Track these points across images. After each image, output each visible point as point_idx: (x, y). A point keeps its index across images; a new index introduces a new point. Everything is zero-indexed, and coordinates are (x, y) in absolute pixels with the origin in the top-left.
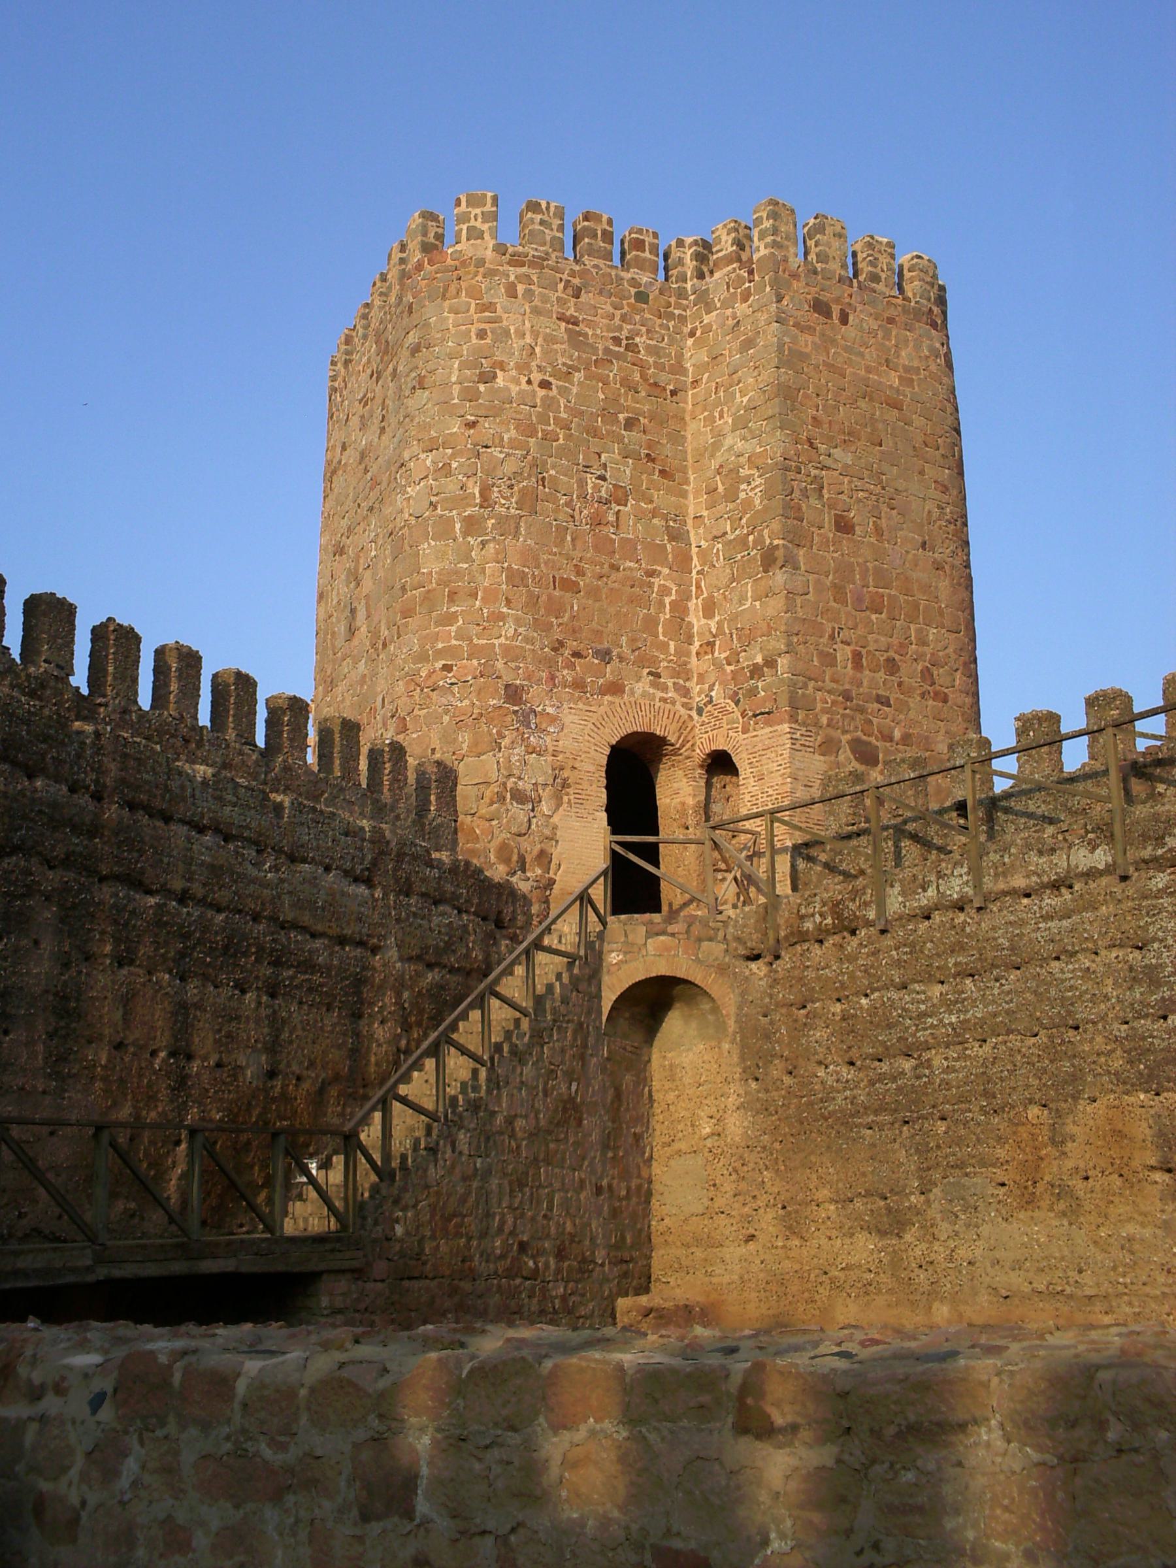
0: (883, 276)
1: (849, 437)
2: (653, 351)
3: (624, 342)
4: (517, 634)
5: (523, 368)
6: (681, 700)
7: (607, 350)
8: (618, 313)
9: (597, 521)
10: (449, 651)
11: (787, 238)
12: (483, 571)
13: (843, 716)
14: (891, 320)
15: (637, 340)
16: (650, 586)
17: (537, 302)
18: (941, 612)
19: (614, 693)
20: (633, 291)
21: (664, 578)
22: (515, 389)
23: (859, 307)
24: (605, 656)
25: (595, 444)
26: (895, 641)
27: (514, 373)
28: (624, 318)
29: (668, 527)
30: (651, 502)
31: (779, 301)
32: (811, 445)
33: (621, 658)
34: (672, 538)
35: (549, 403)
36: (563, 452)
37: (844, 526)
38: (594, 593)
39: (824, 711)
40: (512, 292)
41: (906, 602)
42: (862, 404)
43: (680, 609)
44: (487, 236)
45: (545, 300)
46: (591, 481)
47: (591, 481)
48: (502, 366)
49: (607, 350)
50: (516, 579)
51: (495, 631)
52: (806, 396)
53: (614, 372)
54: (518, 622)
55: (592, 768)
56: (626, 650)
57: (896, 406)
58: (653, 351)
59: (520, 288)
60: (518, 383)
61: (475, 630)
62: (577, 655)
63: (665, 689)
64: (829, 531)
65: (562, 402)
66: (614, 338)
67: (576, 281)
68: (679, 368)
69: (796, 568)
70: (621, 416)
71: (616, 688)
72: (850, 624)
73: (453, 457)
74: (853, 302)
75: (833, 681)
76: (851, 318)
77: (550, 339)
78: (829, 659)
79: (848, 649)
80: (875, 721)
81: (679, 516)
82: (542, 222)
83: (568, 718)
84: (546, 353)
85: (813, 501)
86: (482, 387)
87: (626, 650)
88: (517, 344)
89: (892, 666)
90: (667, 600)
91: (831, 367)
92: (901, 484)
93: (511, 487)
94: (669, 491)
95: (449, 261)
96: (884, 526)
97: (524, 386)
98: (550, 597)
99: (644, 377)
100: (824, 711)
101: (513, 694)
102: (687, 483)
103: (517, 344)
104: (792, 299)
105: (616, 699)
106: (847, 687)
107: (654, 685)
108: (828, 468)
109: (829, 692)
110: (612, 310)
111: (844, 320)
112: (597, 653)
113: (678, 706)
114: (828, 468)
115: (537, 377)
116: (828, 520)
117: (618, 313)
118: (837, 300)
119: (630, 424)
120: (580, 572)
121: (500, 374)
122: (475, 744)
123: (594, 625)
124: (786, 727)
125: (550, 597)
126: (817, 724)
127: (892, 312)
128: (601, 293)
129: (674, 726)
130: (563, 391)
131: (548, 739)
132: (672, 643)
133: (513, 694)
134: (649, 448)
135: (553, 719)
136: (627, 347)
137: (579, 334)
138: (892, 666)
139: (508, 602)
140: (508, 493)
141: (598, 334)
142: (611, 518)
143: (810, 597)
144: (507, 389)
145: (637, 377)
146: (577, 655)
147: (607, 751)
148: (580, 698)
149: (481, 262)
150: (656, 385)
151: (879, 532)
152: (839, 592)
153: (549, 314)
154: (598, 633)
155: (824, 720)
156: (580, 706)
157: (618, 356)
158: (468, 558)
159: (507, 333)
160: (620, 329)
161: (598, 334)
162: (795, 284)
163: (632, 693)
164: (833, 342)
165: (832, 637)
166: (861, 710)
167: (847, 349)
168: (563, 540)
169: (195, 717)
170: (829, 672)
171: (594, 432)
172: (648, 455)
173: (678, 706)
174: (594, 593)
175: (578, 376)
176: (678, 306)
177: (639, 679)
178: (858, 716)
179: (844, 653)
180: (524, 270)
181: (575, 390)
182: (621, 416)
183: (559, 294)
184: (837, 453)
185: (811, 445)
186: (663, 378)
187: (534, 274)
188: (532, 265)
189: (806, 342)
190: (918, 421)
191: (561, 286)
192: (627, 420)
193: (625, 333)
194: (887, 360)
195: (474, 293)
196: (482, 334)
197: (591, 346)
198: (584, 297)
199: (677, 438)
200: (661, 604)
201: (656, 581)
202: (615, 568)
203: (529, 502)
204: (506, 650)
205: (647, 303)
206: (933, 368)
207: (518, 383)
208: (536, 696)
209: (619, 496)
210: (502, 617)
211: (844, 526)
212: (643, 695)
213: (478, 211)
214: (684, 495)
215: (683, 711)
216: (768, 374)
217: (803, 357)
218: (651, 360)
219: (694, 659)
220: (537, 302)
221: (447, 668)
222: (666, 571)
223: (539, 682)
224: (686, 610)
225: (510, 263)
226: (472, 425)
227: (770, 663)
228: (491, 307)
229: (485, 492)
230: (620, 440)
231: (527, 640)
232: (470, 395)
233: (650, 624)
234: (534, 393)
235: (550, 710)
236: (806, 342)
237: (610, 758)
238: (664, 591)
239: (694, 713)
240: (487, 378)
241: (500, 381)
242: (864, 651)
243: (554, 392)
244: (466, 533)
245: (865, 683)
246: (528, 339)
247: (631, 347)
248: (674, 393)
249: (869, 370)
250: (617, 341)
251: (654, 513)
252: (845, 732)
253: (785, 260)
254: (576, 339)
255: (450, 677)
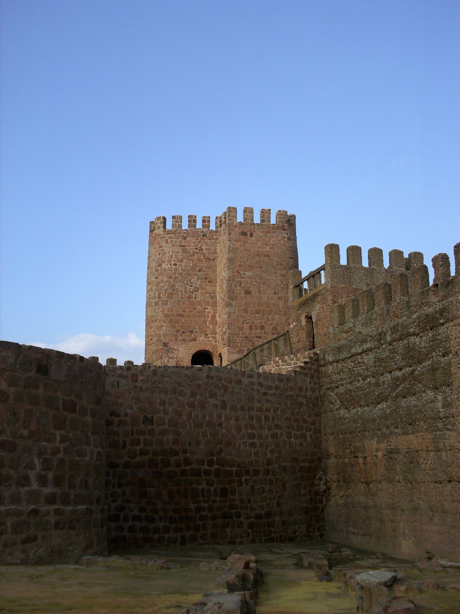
0: (266, 220)
1: (251, 268)
2: (208, 249)
3: (199, 249)
4: (166, 330)
5: (169, 261)
6: (213, 340)
7: (194, 252)
8: (197, 241)
9: (190, 297)
10: (152, 335)
11: (233, 217)
12: (158, 315)
13: (245, 343)
14: (268, 232)
15: (203, 247)
16: (205, 312)
17: (174, 243)
18: (280, 311)
19: (194, 341)
20: (202, 234)
21: (209, 309)
22: (167, 267)
23: (257, 231)
24: (191, 332)
25: (189, 278)
26: (264, 321)
27: (167, 263)
28: (199, 243)
29: (210, 296)
30: (206, 290)
31: (230, 234)
32: (238, 272)
33: (196, 332)
34: (212, 298)
35: (176, 269)
36: (180, 281)
37: (248, 292)
38: (188, 316)
39: (239, 343)
40: (167, 242)
41: (268, 310)
42: (256, 258)
43: (214, 317)
44: (161, 228)
45: (176, 242)
46: (188, 287)
47: (188, 287)
48: (164, 262)
49: (194, 252)
50: (166, 316)
51: (161, 330)
52: (237, 259)
53: (195, 257)
54: (167, 326)
55: (187, 361)
56: (198, 330)
57: (268, 256)
58: (208, 249)
59: (169, 240)
60: (168, 265)
61: (156, 330)
62: (183, 332)
63: (209, 338)
64: (243, 295)
65: (180, 268)
66: (195, 248)
67: (185, 235)
68: (215, 252)
69: (232, 306)
70: (197, 269)
71: (194, 340)
72: (249, 318)
73: (153, 286)
74: (255, 230)
75: (242, 334)
76: (254, 234)
77: (177, 252)
78: (242, 329)
79: (248, 325)
80: (256, 343)
81: (214, 292)
82: (176, 221)
83: (181, 349)
84: (176, 256)
85: (238, 288)
86: (159, 268)
87: (198, 330)
88: (168, 255)
89: (262, 328)
90: (210, 315)
91: (246, 250)
92: (268, 277)
93: (166, 293)
94: (211, 286)
95: (154, 235)
96: (261, 290)
97: (169, 266)
98: (176, 319)
99: (204, 257)
100: (239, 343)
101: (165, 345)
102: (217, 283)
103: (168, 255)
104: (234, 234)
105: (194, 342)
106: (247, 335)
107: (205, 337)
108: (244, 278)
109: (241, 337)
110: (195, 241)
111: (251, 235)
112: (189, 331)
113: (213, 342)
114: (244, 278)
115: (173, 263)
116: (243, 292)
117: (197, 241)
118: (250, 230)
119: (200, 270)
120: (184, 311)
121: (163, 264)
122: (156, 358)
123: (189, 324)
124: (227, 348)
125: (176, 319)
126: (237, 346)
127: (269, 229)
128: (192, 237)
129: (211, 347)
130: (180, 265)
131: (175, 355)
132: (211, 326)
133: (165, 345)
134: (205, 275)
135: (176, 350)
136: (199, 250)
137: (186, 249)
138: (262, 328)
139: (164, 322)
140: (165, 294)
141: (191, 248)
142: (194, 296)
143: (236, 313)
144: (165, 267)
145: (202, 257)
146: (183, 332)
147: (192, 356)
148: (184, 343)
149: (160, 235)
150: (208, 258)
151: (259, 292)
152: (246, 311)
153: (177, 246)
154: (190, 326)
155: (239, 345)
156: (184, 345)
157: (197, 253)
158: (155, 312)
159: (165, 252)
160: (198, 245)
161: (191, 248)
162: (235, 229)
163: (199, 340)
164: (247, 243)
165: (243, 323)
166: (251, 341)
167: (251, 244)
168: (180, 304)
169: (360, 262)
170: (241, 332)
171: (189, 274)
172: (205, 278)
173: (213, 342)
174: (188, 316)
175: (184, 261)
176: (215, 235)
177: (201, 336)
178: (250, 343)
179: (246, 326)
180: (170, 235)
181: (184, 264)
182: (197, 269)
183: (180, 240)
184: (247, 273)
185: (238, 272)
186: (210, 256)
187: (173, 236)
188: (172, 233)
189: (238, 245)
190: (276, 259)
191: (181, 237)
192: (199, 270)
193: (199, 246)
194: (266, 244)
195: (159, 243)
196: (159, 254)
197: (189, 252)
198: (187, 239)
199: (214, 271)
200: (208, 316)
201: (206, 310)
202: (195, 309)
203: (170, 296)
204: (164, 334)
205: (206, 237)
206: (282, 242)
207: (168, 265)
208: (172, 345)
209: (197, 290)
210: (163, 326)
211: (248, 292)
212: (202, 340)
213: (159, 221)
214: (216, 286)
215: (214, 343)
216: (226, 256)
217: (237, 249)
218: (207, 252)
219: (217, 329)
220: (174, 243)
221: (151, 339)
222: (210, 307)
223: (173, 341)
224: (216, 317)
225: (167, 234)
226: (156, 278)
227: (226, 331)
228: (161, 247)
229: (159, 295)
230: (197, 275)
231: (169, 331)
232: (157, 270)
233: (205, 322)
234: (172, 267)
235: (175, 347)
236: (238, 245)
237: (192, 357)
238: (209, 312)
239: (217, 343)
240: (160, 265)
241: (163, 266)
242: (253, 325)
243: (178, 266)
244: (155, 306)
245: (253, 333)
246: (171, 254)
247: (201, 250)
248: (213, 260)
249: (259, 248)
250: (197, 249)
251: (206, 293)
252: (245, 347)
253: (233, 223)
254: (184, 251)
255: (152, 342)
